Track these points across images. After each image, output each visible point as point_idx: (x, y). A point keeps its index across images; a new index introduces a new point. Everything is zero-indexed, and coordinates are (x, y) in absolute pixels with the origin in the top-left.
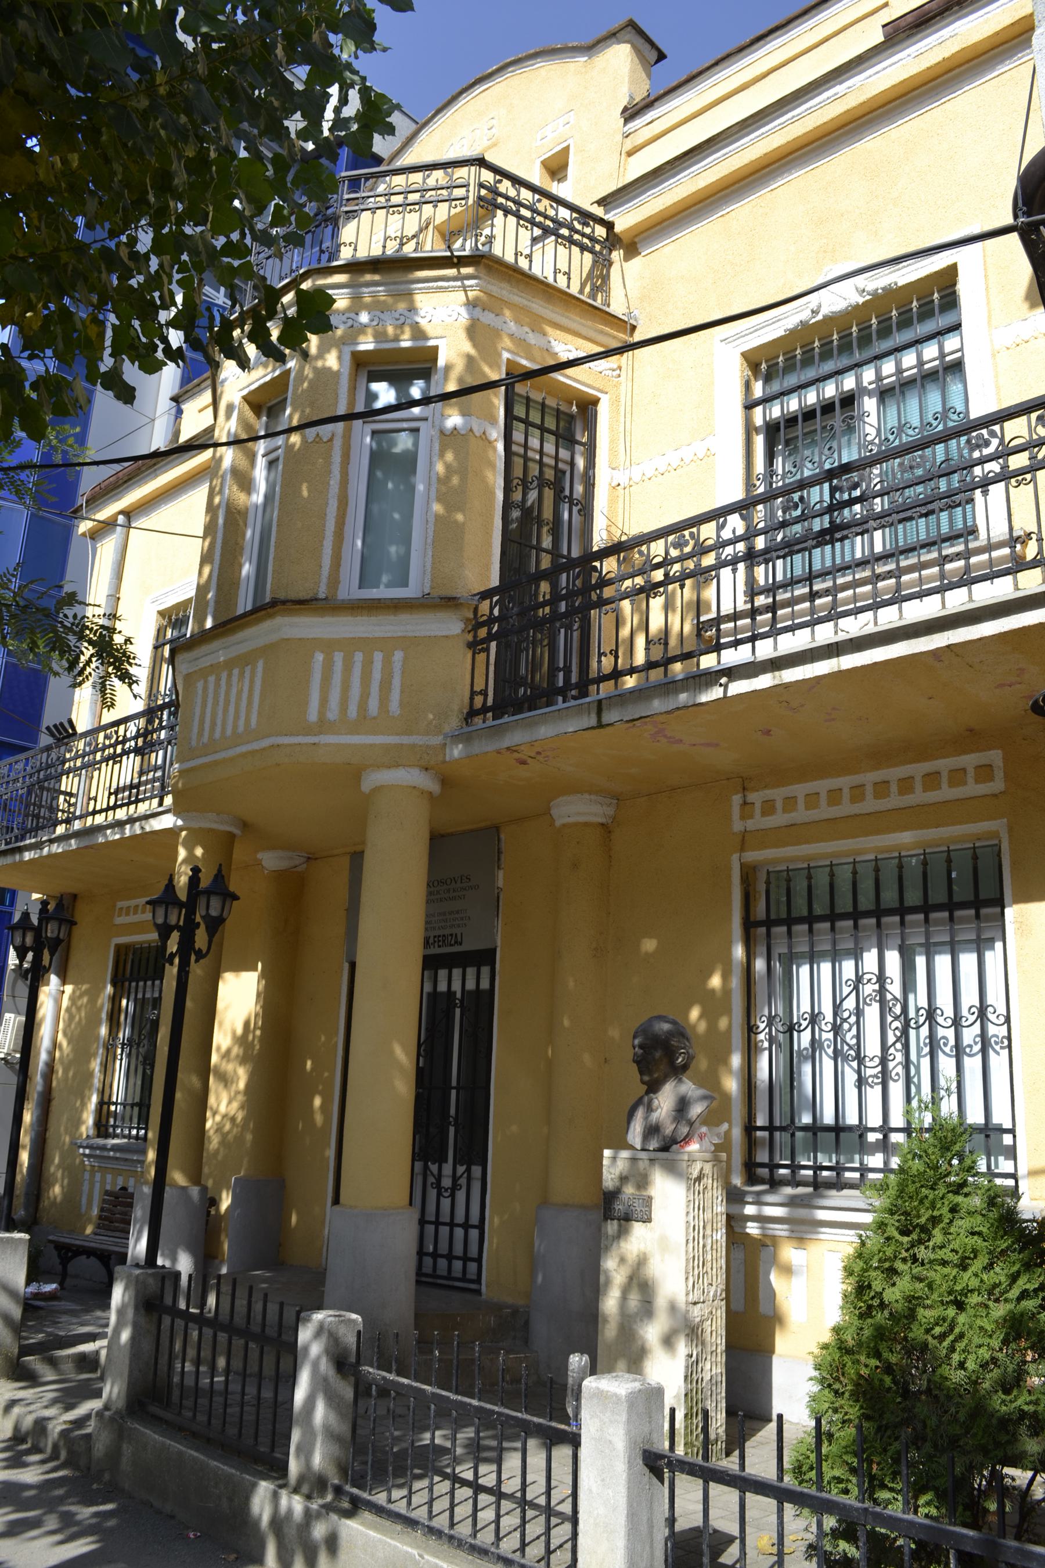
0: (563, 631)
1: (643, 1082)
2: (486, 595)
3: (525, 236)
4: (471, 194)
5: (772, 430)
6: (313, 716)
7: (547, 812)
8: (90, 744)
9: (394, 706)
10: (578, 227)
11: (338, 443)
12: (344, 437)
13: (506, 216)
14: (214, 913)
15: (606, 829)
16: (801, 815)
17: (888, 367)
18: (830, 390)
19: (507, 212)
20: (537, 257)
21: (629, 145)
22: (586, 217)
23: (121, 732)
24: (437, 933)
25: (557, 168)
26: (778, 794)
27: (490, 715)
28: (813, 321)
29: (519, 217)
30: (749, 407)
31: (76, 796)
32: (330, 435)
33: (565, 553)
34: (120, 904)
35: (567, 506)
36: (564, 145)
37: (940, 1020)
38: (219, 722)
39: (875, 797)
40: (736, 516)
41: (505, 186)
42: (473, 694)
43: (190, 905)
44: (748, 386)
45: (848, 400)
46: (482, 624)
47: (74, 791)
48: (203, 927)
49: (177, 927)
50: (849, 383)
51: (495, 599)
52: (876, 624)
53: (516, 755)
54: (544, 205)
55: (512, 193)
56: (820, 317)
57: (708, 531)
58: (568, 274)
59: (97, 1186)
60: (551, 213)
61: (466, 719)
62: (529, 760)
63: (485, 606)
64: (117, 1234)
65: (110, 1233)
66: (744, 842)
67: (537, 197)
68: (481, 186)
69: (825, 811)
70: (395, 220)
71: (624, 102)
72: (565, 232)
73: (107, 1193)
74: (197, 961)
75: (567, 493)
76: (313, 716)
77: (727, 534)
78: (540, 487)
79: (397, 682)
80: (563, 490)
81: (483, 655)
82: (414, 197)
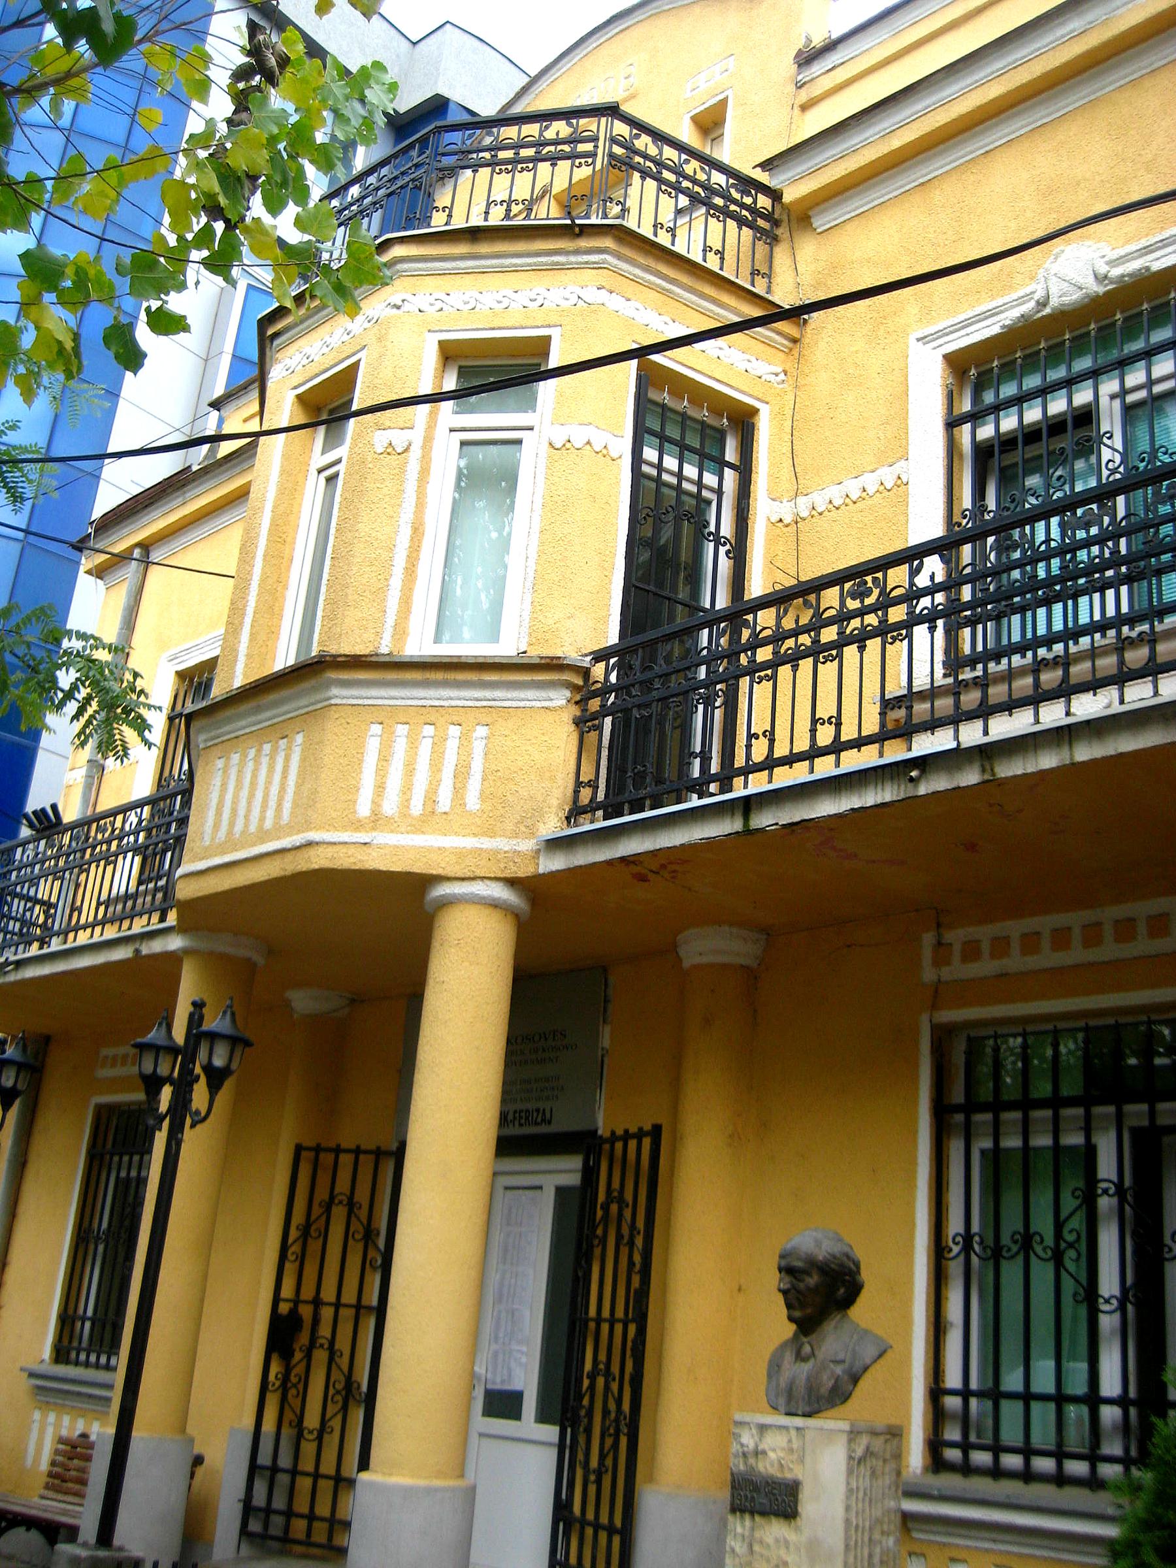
0: (701, 707)
1: (791, 1319)
2: (600, 656)
3: (667, 205)
4: (600, 151)
5: (983, 453)
6: (364, 809)
7: (673, 948)
8: (78, 838)
9: (473, 801)
10: (736, 195)
11: (416, 453)
12: (424, 447)
13: (643, 179)
14: (218, 1062)
15: (750, 976)
16: (1015, 962)
17: (1135, 377)
18: (1058, 405)
19: (645, 174)
20: (682, 233)
21: (803, 96)
22: (747, 184)
23: (118, 824)
24: (520, 1106)
25: (711, 123)
26: (984, 933)
27: (600, 813)
28: (1040, 315)
29: (660, 181)
30: (952, 424)
31: (56, 906)
32: (405, 445)
33: (708, 606)
34: (104, 1052)
35: (712, 545)
36: (721, 97)
37: (1038, 1249)
38: (242, 812)
39: (1117, 940)
40: (936, 557)
41: (644, 142)
42: (578, 784)
43: (188, 1052)
44: (950, 400)
45: (1085, 417)
46: (595, 694)
47: (53, 900)
48: (203, 1080)
49: (169, 1080)
50: (1083, 396)
51: (612, 661)
52: (1122, 702)
53: (636, 869)
54: (692, 167)
55: (653, 151)
56: (1047, 311)
57: (898, 576)
58: (721, 253)
59: (50, 1430)
60: (702, 177)
61: (568, 819)
62: (651, 876)
63: (599, 670)
64: (70, 1499)
65: (60, 1497)
66: (937, 995)
67: (684, 157)
68: (614, 141)
69: (1048, 958)
70: (502, 181)
71: (800, 44)
72: (719, 201)
73: (61, 1440)
74: (193, 1126)
75: (712, 528)
76: (364, 809)
77: (922, 581)
78: (678, 521)
79: (477, 766)
80: (706, 524)
81: (594, 735)
82: (529, 152)
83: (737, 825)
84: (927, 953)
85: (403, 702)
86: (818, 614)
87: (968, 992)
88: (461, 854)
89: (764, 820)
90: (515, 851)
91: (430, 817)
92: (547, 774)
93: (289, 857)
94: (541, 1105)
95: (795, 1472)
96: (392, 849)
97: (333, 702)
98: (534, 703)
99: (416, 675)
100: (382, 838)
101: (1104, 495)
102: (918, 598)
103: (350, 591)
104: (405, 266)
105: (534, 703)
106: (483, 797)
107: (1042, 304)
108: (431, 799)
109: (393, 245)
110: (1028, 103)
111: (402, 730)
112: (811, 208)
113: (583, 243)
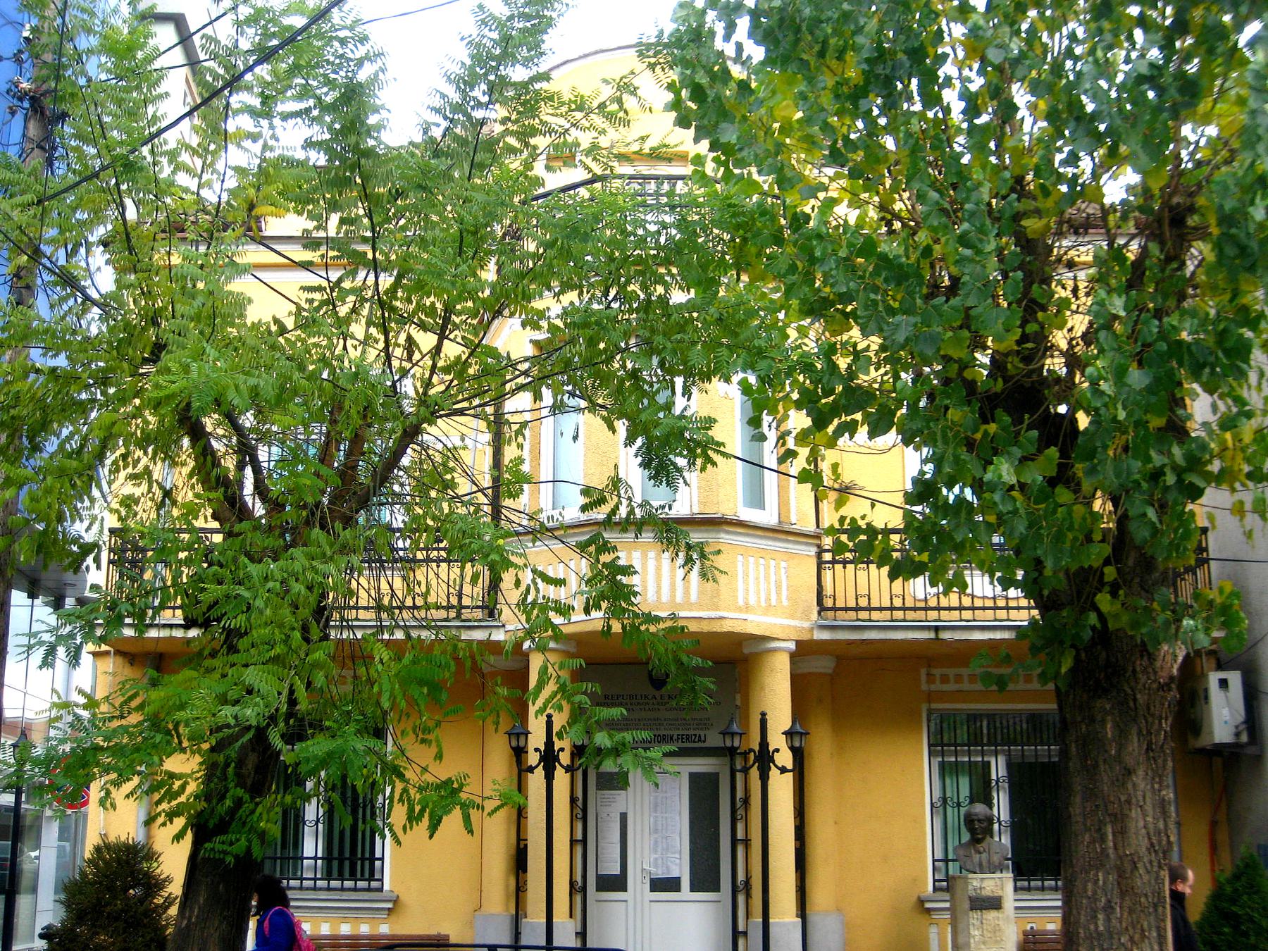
16: (966, 686)
66: (930, 696)
76: (741, 603)
83: (932, 635)
84: (923, 677)
87: (942, 696)
88: (783, 627)
89: (946, 635)
91: (769, 608)
94: (697, 732)
95: (1000, 893)
96: (754, 623)
99: (760, 533)
100: (750, 617)
106: (788, 598)
108: (768, 599)
111: (751, 560)
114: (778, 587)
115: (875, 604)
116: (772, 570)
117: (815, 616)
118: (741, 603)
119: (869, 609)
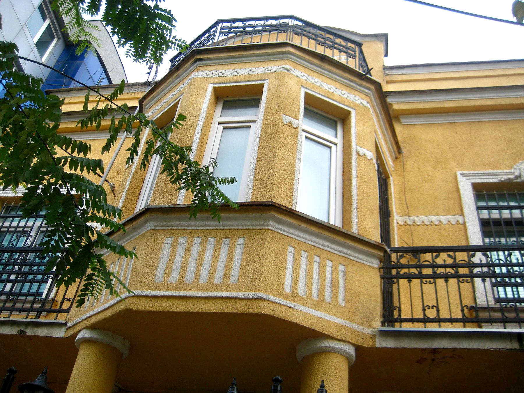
28: (515, 181)
76: (287, 289)
85: (305, 241)
86: (25, 259)
88: (339, 327)
89: (29, 332)
90: (362, 333)
91: (320, 304)
92: (374, 298)
93: (250, 303)
96: (305, 314)
97: (269, 228)
98: (364, 262)
101: (27, 250)
102: (34, 265)
103: (275, 178)
104: (292, 57)
105: (364, 262)
106: (345, 299)
107: (517, 177)
109: (288, 46)
110: (519, 111)
112: (400, 115)
113: (364, 83)
114: (334, 285)
115: (444, 314)
116: (328, 270)
117: (377, 323)
118: (287, 289)
119: (439, 320)
